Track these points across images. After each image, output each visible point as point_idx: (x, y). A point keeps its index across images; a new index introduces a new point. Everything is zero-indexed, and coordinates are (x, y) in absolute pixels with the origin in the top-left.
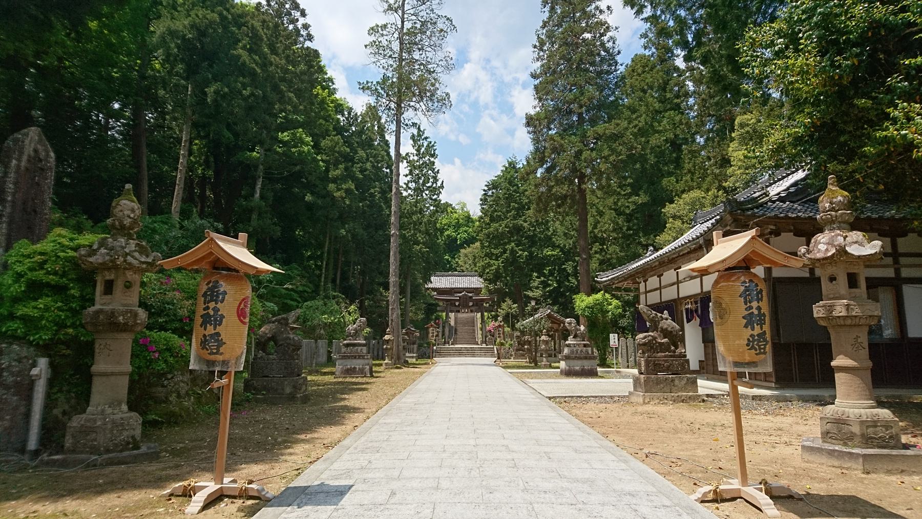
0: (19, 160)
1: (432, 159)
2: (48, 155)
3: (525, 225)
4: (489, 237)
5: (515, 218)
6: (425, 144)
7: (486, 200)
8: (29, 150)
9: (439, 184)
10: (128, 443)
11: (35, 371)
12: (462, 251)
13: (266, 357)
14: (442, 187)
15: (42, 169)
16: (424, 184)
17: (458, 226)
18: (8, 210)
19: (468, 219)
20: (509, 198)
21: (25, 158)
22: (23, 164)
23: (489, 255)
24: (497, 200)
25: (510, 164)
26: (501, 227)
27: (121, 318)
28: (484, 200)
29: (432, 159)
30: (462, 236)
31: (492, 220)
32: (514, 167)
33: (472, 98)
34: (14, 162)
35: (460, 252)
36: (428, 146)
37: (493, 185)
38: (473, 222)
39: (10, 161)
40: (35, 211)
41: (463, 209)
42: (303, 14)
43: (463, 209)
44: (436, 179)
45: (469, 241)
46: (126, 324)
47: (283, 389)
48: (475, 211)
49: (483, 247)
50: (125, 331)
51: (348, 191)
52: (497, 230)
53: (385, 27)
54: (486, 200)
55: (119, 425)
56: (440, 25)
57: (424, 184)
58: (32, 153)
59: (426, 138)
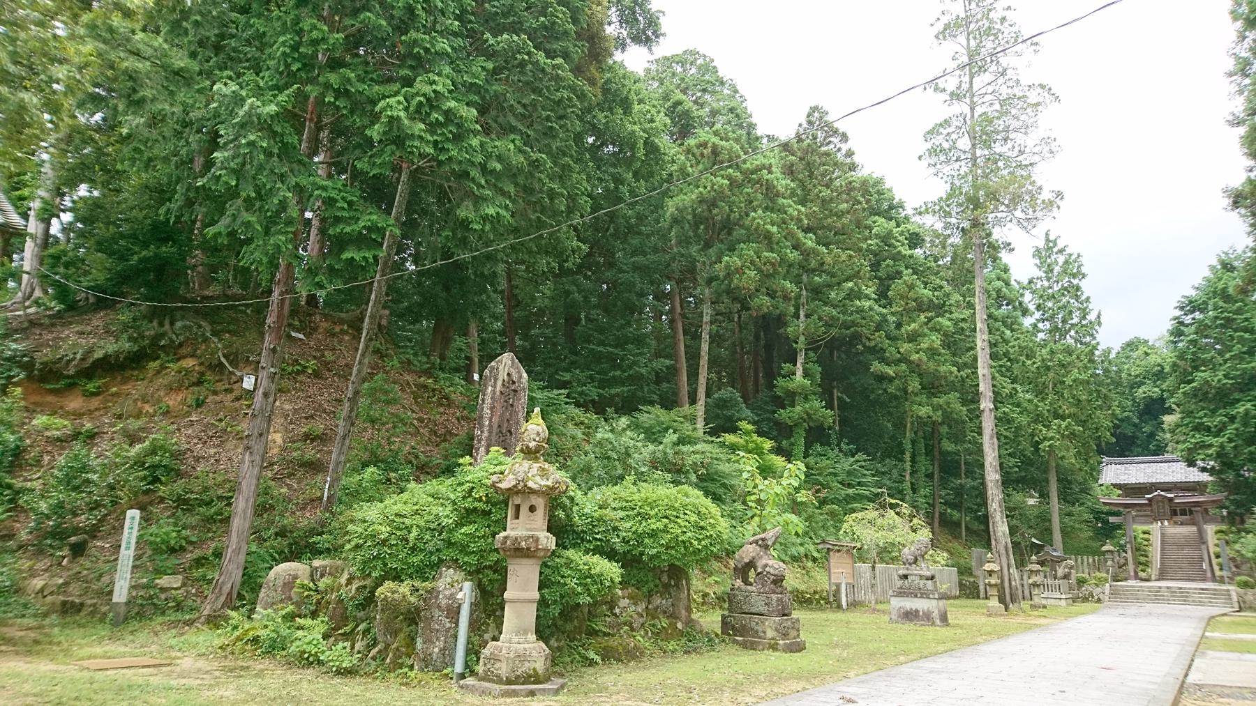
0: (494, 386)
1: (1075, 282)
2: (521, 377)
6: (1061, 259)
8: (502, 375)
10: (530, 676)
11: (460, 596)
13: (743, 587)
15: (515, 391)
16: (1064, 322)
18: (486, 434)
21: (499, 383)
22: (498, 389)
27: (523, 543)
29: (1075, 282)
34: (490, 388)
36: (1066, 262)
37: (1191, 306)
39: (487, 388)
40: (510, 432)
42: (844, 138)
46: (528, 549)
47: (764, 632)
50: (528, 557)
53: (946, 123)
55: (522, 657)
56: (1033, 99)
58: (506, 378)
59: (1061, 251)
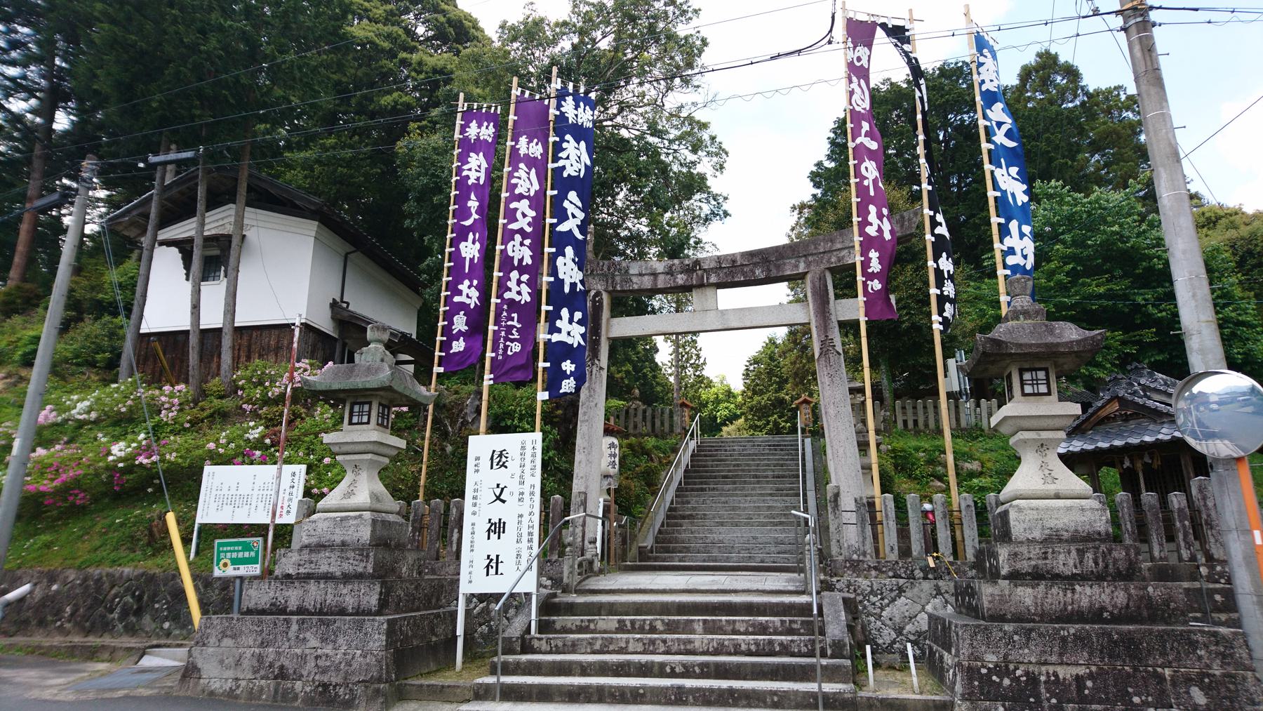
3: (787, 397)
4: (752, 410)
5: (776, 391)
7: (748, 375)
9: (702, 361)
12: (725, 429)
14: (705, 363)
17: (717, 401)
19: (729, 394)
20: (770, 373)
23: (754, 427)
24: (758, 375)
25: (770, 340)
26: (764, 400)
28: (746, 375)
30: (722, 413)
31: (755, 392)
32: (774, 343)
33: (1111, 568)
35: (721, 430)
37: (755, 361)
38: (734, 397)
41: (722, 383)
43: (722, 383)
44: (698, 357)
45: (732, 418)
48: (737, 385)
49: (746, 420)
51: (627, 372)
52: (760, 403)
54: (748, 375)
57: (687, 360)
